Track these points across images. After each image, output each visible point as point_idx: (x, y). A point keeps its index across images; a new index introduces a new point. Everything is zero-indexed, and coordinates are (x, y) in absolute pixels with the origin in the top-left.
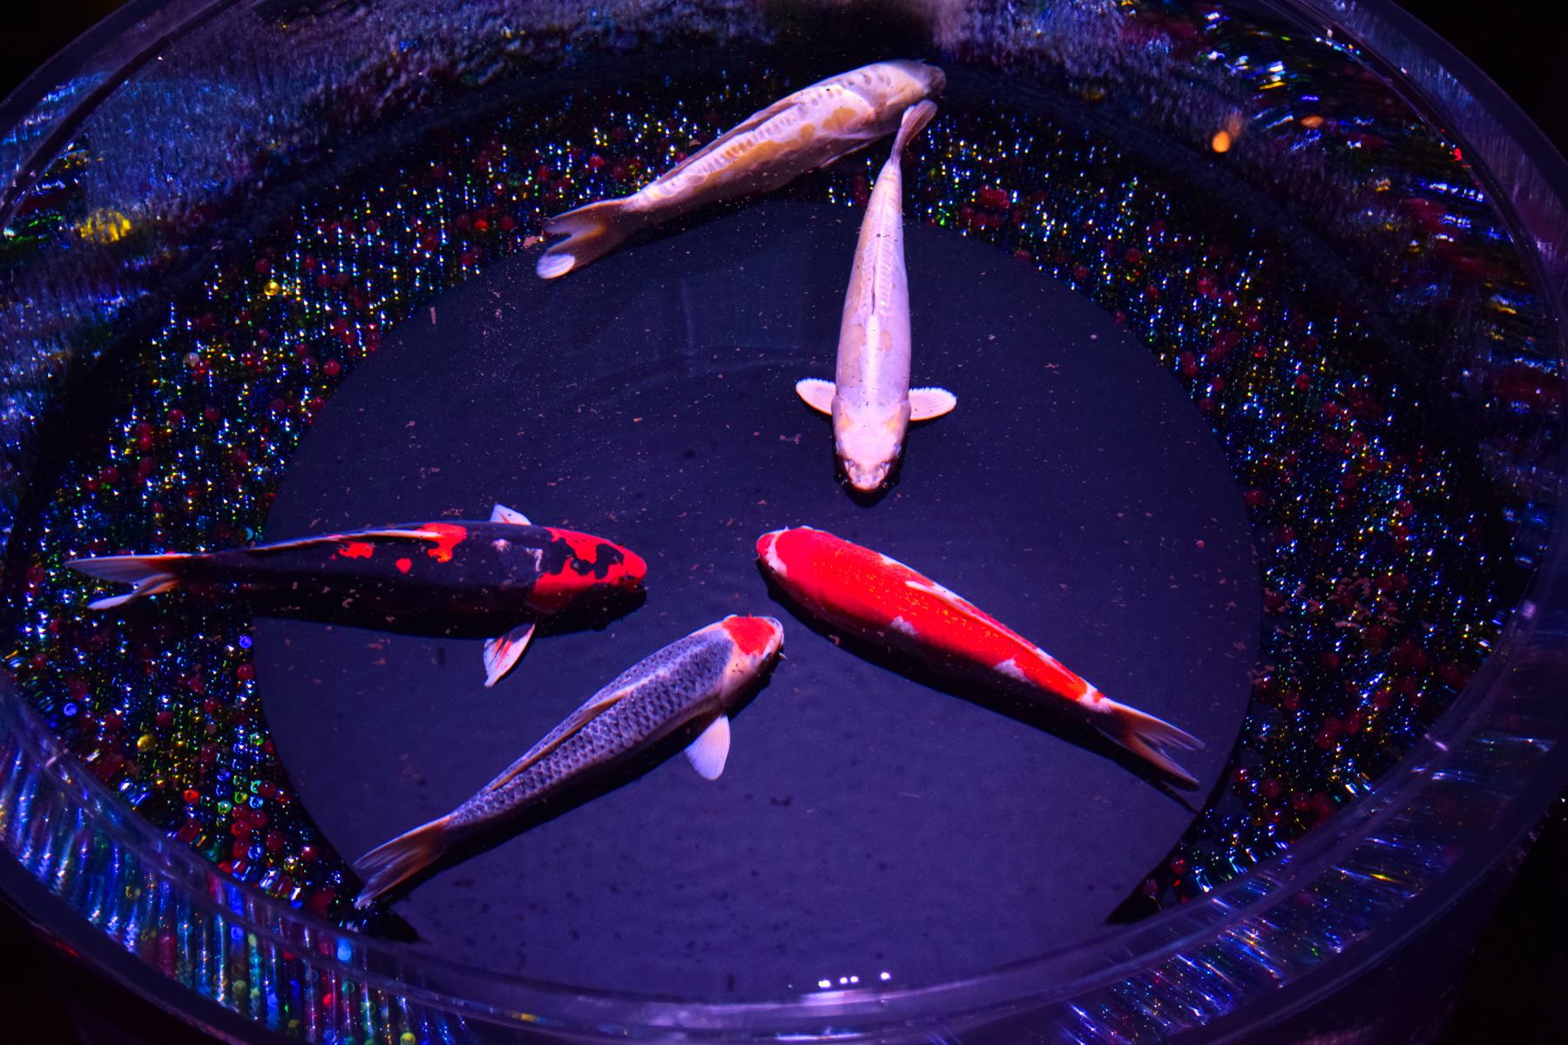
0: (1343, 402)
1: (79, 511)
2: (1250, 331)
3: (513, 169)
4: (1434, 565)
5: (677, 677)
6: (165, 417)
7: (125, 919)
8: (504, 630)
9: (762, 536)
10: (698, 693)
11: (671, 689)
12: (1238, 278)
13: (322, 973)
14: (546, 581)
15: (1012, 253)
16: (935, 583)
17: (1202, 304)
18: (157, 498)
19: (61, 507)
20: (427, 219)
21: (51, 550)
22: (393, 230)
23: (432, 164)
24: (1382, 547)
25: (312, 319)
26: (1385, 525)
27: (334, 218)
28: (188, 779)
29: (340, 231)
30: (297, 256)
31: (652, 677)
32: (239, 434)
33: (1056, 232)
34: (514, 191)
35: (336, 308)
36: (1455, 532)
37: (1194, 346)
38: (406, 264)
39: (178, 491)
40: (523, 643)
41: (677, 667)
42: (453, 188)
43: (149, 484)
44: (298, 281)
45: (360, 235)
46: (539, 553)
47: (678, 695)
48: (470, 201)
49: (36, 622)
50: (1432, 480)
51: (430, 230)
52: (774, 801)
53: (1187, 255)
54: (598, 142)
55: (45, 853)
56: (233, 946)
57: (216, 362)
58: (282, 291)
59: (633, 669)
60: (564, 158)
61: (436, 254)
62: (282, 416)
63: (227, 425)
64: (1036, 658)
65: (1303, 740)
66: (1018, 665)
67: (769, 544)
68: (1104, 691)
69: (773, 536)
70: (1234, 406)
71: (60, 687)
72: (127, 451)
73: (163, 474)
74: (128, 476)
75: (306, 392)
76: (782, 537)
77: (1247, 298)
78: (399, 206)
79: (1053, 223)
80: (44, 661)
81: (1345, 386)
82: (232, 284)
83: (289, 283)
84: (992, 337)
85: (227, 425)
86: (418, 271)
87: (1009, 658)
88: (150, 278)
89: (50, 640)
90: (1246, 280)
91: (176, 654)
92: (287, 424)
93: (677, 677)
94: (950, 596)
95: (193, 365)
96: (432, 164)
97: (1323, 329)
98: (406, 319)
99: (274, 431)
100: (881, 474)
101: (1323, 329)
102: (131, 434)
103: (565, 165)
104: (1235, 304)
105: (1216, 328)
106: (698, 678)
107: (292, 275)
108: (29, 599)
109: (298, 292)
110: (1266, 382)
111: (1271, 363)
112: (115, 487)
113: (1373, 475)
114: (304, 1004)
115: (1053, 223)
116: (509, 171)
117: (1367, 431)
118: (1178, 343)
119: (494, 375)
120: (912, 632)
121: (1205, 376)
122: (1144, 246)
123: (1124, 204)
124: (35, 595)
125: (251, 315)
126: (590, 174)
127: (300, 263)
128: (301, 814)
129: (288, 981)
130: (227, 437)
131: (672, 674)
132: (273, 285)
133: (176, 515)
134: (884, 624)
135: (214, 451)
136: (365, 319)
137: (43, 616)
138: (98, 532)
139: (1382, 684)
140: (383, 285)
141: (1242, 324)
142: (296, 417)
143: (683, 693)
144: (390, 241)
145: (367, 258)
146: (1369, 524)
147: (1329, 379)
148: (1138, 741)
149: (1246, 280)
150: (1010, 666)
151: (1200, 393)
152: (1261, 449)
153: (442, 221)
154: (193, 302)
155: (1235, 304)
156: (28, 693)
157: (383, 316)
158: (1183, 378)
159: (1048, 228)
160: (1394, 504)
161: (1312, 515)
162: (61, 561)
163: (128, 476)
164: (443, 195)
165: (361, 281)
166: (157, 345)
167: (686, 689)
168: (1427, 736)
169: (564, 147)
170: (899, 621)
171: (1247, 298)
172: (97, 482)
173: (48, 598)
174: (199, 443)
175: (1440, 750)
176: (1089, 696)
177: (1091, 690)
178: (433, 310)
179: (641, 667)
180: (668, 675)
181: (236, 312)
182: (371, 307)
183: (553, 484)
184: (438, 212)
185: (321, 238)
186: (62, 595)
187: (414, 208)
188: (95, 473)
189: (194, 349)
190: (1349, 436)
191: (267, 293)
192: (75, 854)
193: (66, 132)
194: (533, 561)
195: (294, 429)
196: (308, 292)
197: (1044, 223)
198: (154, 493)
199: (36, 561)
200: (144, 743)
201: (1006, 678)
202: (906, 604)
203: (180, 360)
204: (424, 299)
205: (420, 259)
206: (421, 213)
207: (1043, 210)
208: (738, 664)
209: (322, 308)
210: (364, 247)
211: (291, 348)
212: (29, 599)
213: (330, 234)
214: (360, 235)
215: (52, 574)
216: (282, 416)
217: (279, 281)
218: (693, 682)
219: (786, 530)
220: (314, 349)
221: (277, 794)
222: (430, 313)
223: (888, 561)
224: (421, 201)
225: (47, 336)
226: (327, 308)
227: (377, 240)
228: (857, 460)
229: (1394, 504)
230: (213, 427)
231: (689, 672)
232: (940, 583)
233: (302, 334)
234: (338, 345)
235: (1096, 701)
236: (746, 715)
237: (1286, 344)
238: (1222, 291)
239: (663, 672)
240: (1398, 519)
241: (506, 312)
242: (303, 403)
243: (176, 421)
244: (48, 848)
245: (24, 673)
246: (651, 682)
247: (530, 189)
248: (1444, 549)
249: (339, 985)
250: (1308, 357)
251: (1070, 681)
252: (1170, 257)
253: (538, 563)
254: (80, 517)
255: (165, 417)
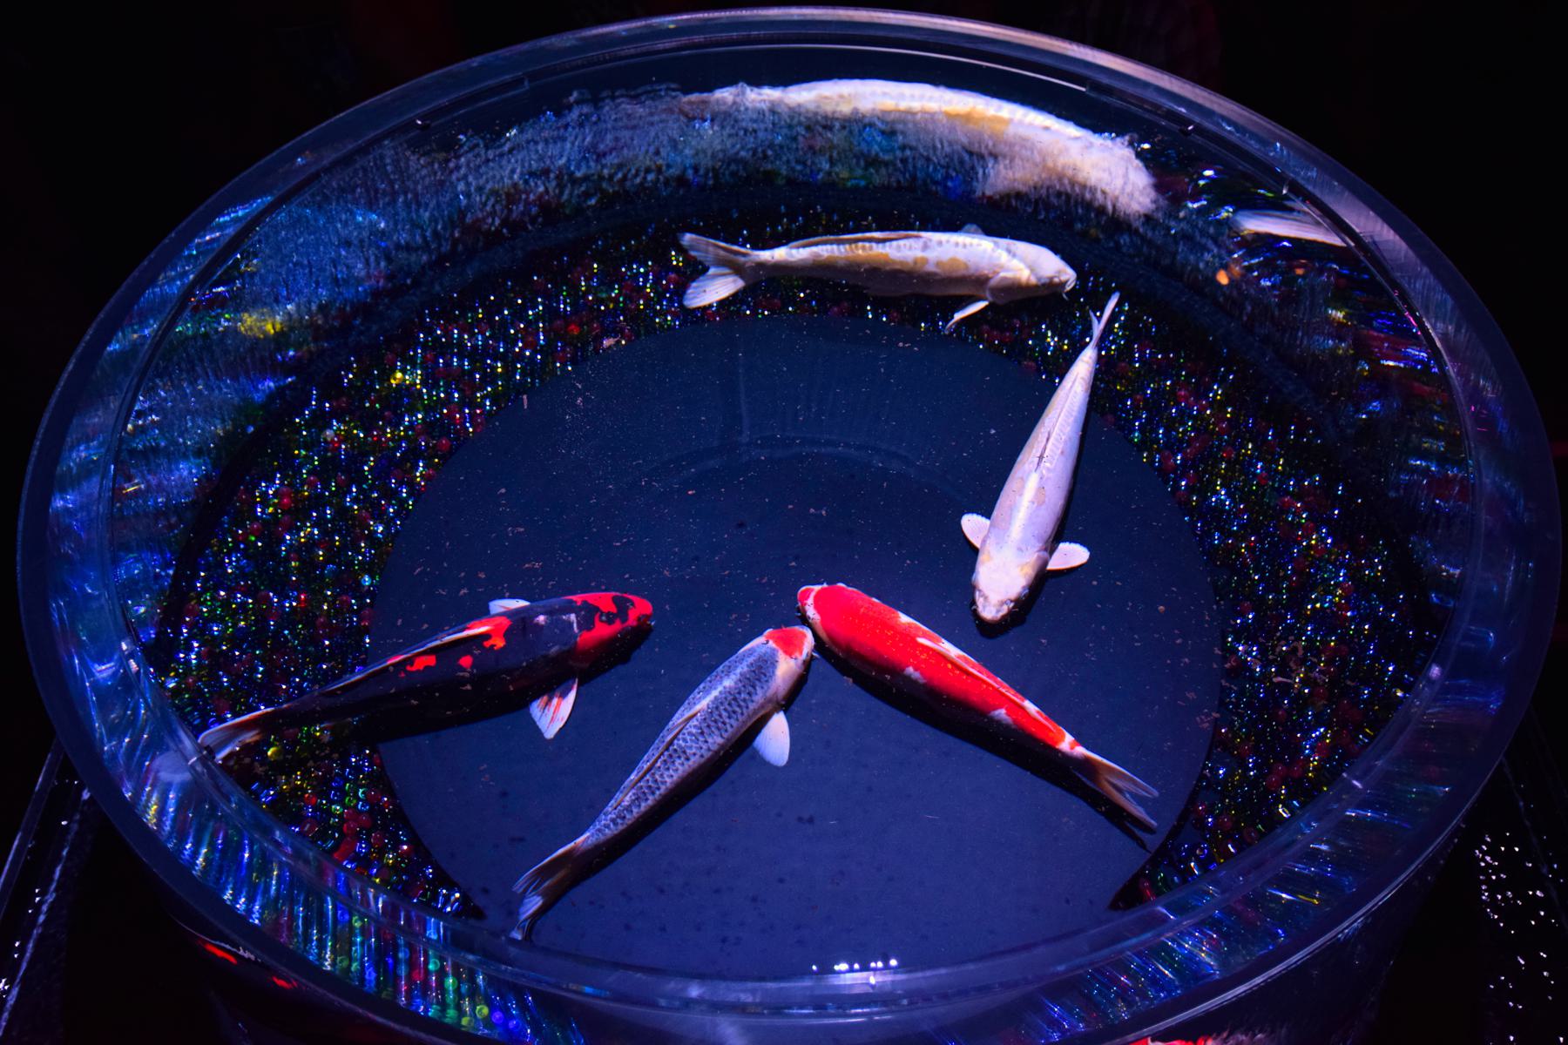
0: (1298, 496)
1: (230, 559)
2: (1220, 434)
3: (601, 283)
4: (1369, 638)
5: (740, 685)
6: (303, 482)
7: (251, 900)
8: (550, 687)
9: (804, 588)
10: (759, 697)
11: (737, 696)
12: (1212, 390)
13: (413, 951)
14: (583, 638)
15: (1020, 363)
16: (943, 640)
17: (1180, 411)
18: (296, 549)
19: (215, 555)
20: (528, 323)
21: (205, 590)
22: (500, 333)
23: (535, 278)
24: (1329, 622)
25: (429, 404)
26: (1331, 601)
27: (451, 321)
28: (308, 784)
29: (456, 331)
30: (419, 351)
31: (720, 688)
32: (362, 499)
33: (1058, 348)
34: (602, 302)
35: (449, 395)
36: (1388, 610)
37: (1173, 446)
38: (509, 360)
39: (312, 544)
40: (572, 696)
41: (738, 676)
42: (550, 298)
43: (288, 537)
44: (419, 372)
45: (472, 336)
46: (573, 617)
47: (744, 700)
48: (565, 308)
49: (190, 649)
50: (1372, 567)
51: (529, 336)
52: (800, 819)
53: (1163, 370)
54: (675, 263)
55: (187, 843)
56: (339, 927)
57: (348, 437)
58: (405, 380)
59: (701, 686)
60: (645, 275)
61: (534, 353)
62: (400, 484)
63: (354, 490)
64: (1022, 708)
65: (1254, 783)
66: (1008, 714)
67: (808, 597)
68: (1080, 740)
69: (812, 590)
70: (1204, 499)
71: (206, 704)
72: (271, 510)
73: (299, 529)
74: (271, 531)
75: (421, 464)
76: (820, 593)
77: (1219, 407)
78: (506, 312)
79: (1056, 339)
80: (195, 682)
81: (1299, 484)
82: (365, 373)
83: (412, 374)
84: (993, 432)
85: (354, 490)
86: (519, 366)
87: (1001, 708)
88: (294, 367)
89: (199, 666)
90: (1218, 391)
91: (303, 679)
92: (404, 490)
93: (740, 685)
94: (952, 651)
95: (329, 439)
96: (535, 278)
97: (1281, 434)
98: (506, 405)
99: (392, 495)
100: (1005, 610)
101: (1281, 434)
102: (275, 495)
103: (645, 282)
104: (1208, 412)
105: (1191, 432)
106: (757, 683)
107: (414, 367)
108: (185, 631)
109: (418, 381)
110: (1231, 479)
111: (1237, 461)
112: (258, 539)
113: (1321, 559)
114: (397, 978)
115: (1056, 339)
116: (599, 285)
117: (1316, 522)
118: (1158, 443)
119: (573, 453)
120: (922, 681)
121: (1182, 472)
122: (1133, 361)
123: (1117, 325)
124: (190, 626)
125: (378, 400)
126: (667, 289)
127: (422, 357)
128: (400, 818)
129: (383, 956)
130: (355, 500)
131: (736, 683)
132: (399, 375)
133: (309, 565)
134: (897, 672)
135: (342, 512)
136: (472, 404)
137: (196, 645)
138: (244, 577)
139: (1323, 736)
140: (489, 378)
141: (1214, 429)
142: (411, 484)
143: (747, 697)
144: (497, 341)
145: (476, 355)
146: (1316, 600)
147: (1286, 476)
148: (1106, 784)
149: (1218, 391)
150: (1001, 713)
151: (1177, 487)
152: (1225, 533)
153: (541, 325)
154: (331, 388)
155: (1208, 412)
156: (179, 708)
157: (488, 403)
158: (1163, 472)
159: (1052, 344)
160: (1338, 585)
161: (1267, 591)
162: (213, 599)
163: (271, 531)
164: (542, 304)
165: (471, 373)
166: (300, 423)
167: (749, 694)
168: (1345, 775)
169: (645, 265)
170: (910, 670)
171: (1219, 407)
172: (246, 534)
173: (201, 630)
174: (331, 506)
175: (1356, 787)
176: (1067, 743)
177: (1069, 738)
178: (525, 397)
179: (708, 684)
180: (732, 684)
181: (367, 397)
182: (478, 395)
183: (618, 544)
184: (537, 317)
185: (440, 337)
186: (211, 627)
187: (519, 314)
188: (243, 527)
189: (331, 427)
190: (1300, 526)
191: (393, 381)
192: (212, 846)
193: (234, 244)
194: (571, 624)
195: (410, 494)
196: (430, 380)
197: (1049, 340)
198: (291, 545)
199: (193, 599)
200: (274, 753)
201: (999, 722)
202: (916, 658)
203: (318, 436)
204: (521, 388)
205: (521, 355)
206: (524, 318)
207: (1047, 329)
208: (786, 668)
209: (438, 395)
210: (475, 347)
211: (411, 426)
212: (185, 631)
213: (447, 333)
214: (472, 336)
215: (205, 610)
216: (400, 484)
217: (404, 372)
218: (754, 687)
219: (825, 585)
220: (429, 428)
221: (381, 800)
222: (522, 399)
223: (904, 619)
224: (524, 308)
225: (208, 413)
226: (442, 395)
227: (485, 339)
228: (987, 592)
229: (1338, 585)
230: (343, 491)
231: (749, 679)
232: (949, 641)
233: (420, 416)
234: (449, 425)
235: (1072, 748)
236: (795, 708)
237: (1250, 447)
238: (1198, 398)
239: (728, 683)
240: (1341, 597)
241: (586, 400)
242: (418, 474)
243: (312, 485)
244: (191, 839)
245: (176, 692)
246: (720, 693)
247: (616, 300)
248: (1379, 623)
249: (426, 962)
250: (1269, 458)
251: (1051, 730)
252: (1155, 370)
253: (575, 625)
254: (230, 563)
255: (303, 482)
